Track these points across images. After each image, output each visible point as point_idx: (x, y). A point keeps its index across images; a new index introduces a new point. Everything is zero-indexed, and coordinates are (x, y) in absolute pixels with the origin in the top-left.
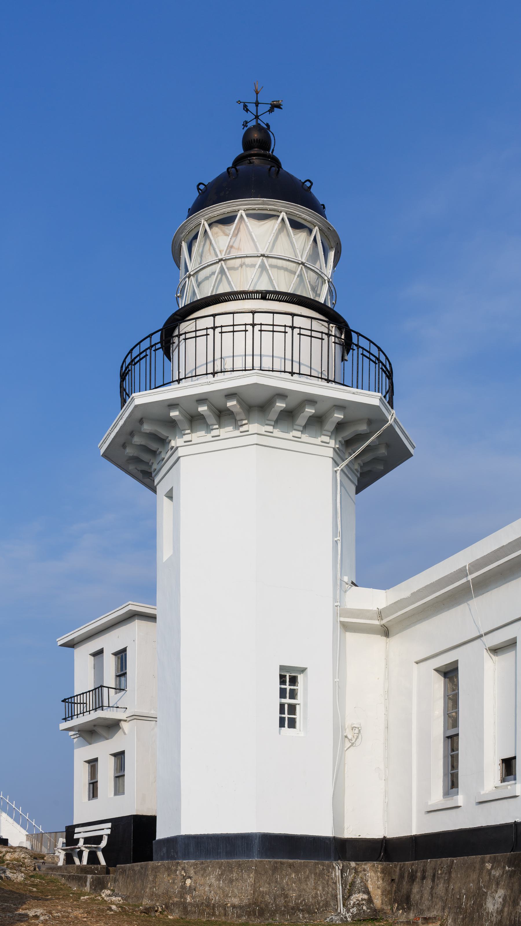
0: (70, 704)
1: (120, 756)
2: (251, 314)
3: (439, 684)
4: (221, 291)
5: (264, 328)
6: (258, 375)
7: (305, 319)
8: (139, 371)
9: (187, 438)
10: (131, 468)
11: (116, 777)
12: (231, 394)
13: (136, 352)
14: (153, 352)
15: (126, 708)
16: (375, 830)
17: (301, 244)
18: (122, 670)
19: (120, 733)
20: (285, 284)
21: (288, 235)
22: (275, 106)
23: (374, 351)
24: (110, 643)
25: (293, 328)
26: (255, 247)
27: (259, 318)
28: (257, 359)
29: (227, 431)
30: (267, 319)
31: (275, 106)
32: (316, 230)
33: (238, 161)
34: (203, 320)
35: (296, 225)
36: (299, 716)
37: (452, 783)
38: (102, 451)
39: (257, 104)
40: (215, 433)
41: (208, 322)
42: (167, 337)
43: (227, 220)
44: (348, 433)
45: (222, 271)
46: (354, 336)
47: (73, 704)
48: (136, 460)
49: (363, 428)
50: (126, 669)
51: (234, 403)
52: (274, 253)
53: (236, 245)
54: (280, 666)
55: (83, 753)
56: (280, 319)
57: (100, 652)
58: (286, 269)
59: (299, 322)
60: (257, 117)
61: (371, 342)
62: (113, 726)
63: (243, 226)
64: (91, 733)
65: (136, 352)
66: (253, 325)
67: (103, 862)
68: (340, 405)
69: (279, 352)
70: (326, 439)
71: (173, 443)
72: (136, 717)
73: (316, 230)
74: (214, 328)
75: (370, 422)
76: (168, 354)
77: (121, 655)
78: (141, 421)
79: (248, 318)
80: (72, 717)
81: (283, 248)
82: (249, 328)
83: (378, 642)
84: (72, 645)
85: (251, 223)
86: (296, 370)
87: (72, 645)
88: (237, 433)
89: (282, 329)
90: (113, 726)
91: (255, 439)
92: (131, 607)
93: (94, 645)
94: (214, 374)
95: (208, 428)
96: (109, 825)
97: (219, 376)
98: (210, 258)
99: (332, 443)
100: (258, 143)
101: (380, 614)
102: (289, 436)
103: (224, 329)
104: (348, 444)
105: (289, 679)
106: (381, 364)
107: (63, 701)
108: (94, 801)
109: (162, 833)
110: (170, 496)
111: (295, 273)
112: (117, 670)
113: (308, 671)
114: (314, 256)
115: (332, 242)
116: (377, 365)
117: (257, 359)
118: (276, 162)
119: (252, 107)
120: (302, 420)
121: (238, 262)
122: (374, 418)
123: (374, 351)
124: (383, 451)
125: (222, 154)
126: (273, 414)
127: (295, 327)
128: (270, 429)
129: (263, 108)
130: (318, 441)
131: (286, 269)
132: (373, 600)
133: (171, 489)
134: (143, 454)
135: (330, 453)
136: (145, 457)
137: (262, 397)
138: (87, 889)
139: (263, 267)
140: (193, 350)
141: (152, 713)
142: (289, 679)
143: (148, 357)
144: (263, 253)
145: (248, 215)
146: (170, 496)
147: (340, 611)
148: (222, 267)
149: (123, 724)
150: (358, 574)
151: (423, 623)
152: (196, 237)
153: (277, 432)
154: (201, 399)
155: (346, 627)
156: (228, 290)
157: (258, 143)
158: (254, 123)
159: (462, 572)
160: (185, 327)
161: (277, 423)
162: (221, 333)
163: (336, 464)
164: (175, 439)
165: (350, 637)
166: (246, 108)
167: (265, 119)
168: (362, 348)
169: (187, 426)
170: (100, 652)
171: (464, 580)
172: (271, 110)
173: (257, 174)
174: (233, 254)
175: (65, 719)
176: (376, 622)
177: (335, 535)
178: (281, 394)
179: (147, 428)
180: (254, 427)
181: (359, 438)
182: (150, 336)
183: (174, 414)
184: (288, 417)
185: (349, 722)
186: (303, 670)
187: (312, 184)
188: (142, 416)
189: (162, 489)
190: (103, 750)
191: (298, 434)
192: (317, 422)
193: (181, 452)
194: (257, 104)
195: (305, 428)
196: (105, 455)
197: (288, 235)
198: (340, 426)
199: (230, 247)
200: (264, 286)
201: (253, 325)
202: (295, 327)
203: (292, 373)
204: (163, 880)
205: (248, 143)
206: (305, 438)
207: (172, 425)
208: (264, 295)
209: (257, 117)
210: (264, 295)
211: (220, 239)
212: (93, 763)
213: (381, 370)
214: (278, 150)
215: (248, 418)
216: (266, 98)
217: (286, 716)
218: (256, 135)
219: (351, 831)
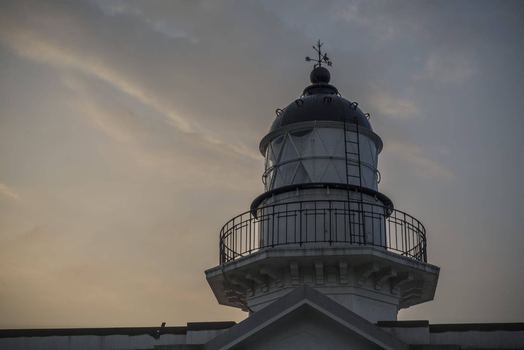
0: (361, 210)
2: (299, 204)
5: (308, 212)
14: (235, 231)
30: (283, 208)
31: (308, 59)
41: (270, 210)
47: (361, 210)
61: (413, 218)
65: (225, 230)
74: (301, 211)
79: (297, 207)
89: (323, 212)
100: (320, 78)
103: (281, 215)
106: (407, 224)
116: (403, 226)
123: (416, 224)
127: (332, 209)
143: (232, 234)
144: (331, 155)
145: (292, 135)
157: (320, 78)
162: (278, 217)
168: (408, 223)
187: (357, 104)
202: (332, 209)
213: (407, 229)
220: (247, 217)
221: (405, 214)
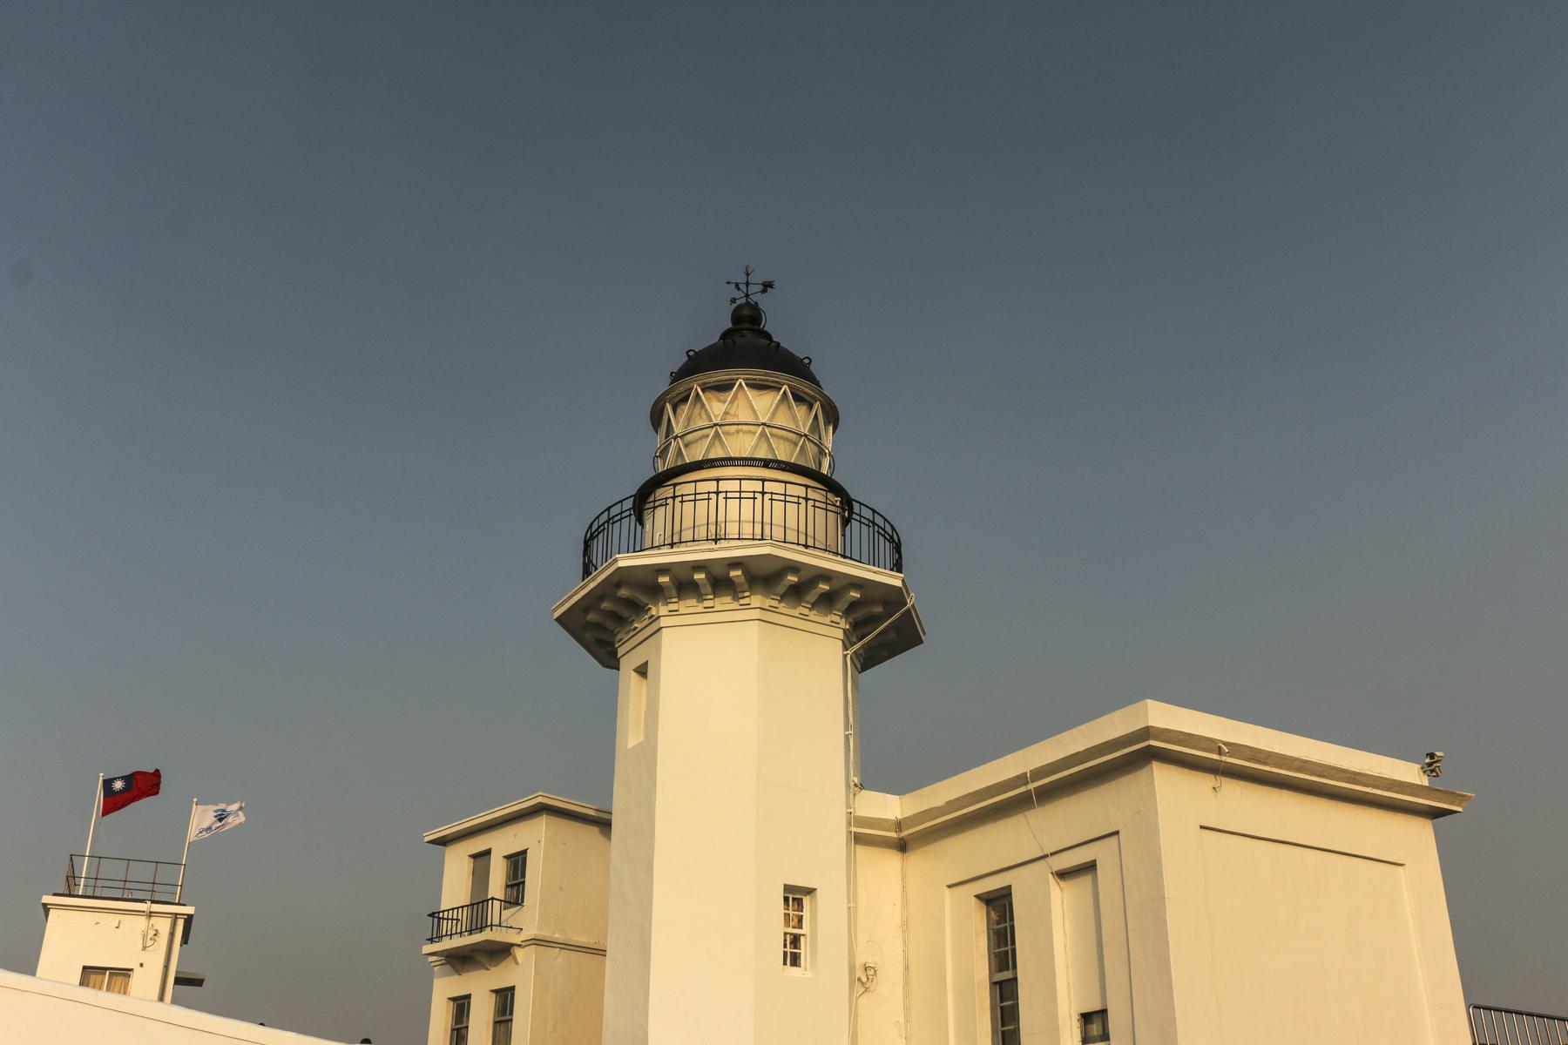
1: (505, 998)
3: (977, 922)
4: (712, 456)
6: (772, 545)
7: (796, 487)
8: (598, 546)
9: (672, 607)
10: (588, 635)
11: (496, 1023)
12: (735, 563)
15: (1117, 833)
17: (801, 418)
18: (515, 877)
19: (509, 961)
20: (783, 454)
21: (790, 407)
22: (767, 286)
24: (502, 844)
26: (748, 415)
27: (769, 487)
28: (712, 528)
29: (724, 602)
31: (767, 286)
32: (817, 405)
33: (725, 336)
34: (702, 484)
35: (799, 399)
36: (804, 950)
38: (556, 615)
39: (747, 284)
40: (707, 603)
42: (642, 500)
43: (724, 387)
44: (859, 614)
45: (717, 435)
46: (856, 507)
48: (597, 626)
49: (879, 609)
50: (523, 875)
51: (739, 573)
52: (774, 423)
53: (732, 412)
55: (445, 987)
57: (488, 853)
58: (787, 439)
59: (811, 494)
62: (500, 952)
63: (740, 395)
64: (461, 960)
66: (763, 493)
68: (859, 584)
69: (792, 523)
70: (837, 619)
71: (654, 612)
72: (537, 942)
73: (817, 405)
74: (717, 493)
75: (886, 604)
76: (640, 521)
77: (517, 862)
78: (618, 585)
81: (782, 420)
83: (892, 860)
84: (444, 842)
85: (749, 392)
86: (810, 543)
87: (444, 842)
88: (735, 605)
90: (500, 952)
91: (756, 614)
92: (540, 800)
93: (477, 844)
94: (716, 540)
95: (700, 597)
97: (723, 544)
98: (704, 423)
99: (844, 624)
100: (747, 319)
101: (899, 825)
102: (796, 612)
104: (856, 626)
105: (795, 896)
110: (642, 671)
111: (796, 444)
112: (508, 878)
113: (818, 892)
114: (815, 427)
115: (832, 415)
117: (767, 528)
118: (768, 336)
119: (743, 287)
120: (812, 596)
121: (734, 428)
122: (893, 599)
123: (867, 513)
124: (893, 636)
125: (711, 328)
126: (781, 589)
128: (775, 603)
129: (752, 289)
130: (827, 620)
131: (787, 439)
132: (888, 807)
133: (646, 664)
134: (608, 622)
135: (840, 634)
136: (610, 624)
139: (763, 434)
140: (658, 521)
142: (795, 896)
146: (642, 671)
147: (853, 820)
148: (717, 433)
149: (519, 954)
150: (862, 777)
151: (930, 847)
152: (685, 399)
153: (782, 607)
154: (698, 566)
155: (859, 839)
156: (722, 455)
157: (747, 319)
158: (743, 301)
159: (1021, 779)
160: (664, 492)
161: (783, 598)
163: (845, 648)
164: (656, 604)
165: (862, 851)
166: (737, 286)
167: (754, 298)
169: (674, 592)
170: (488, 853)
171: (1022, 789)
172: (764, 291)
173: (748, 345)
174: (730, 420)
175: (431, 940)
176: (894, 835)
177: (846, 728)
178: (794, 567)
179: (623, 592)
180: (756, 600)
181: (874, 620)
182: (608, 509)
183: (664, 579)
184: (795, 594)
185: (859, 962)
186: (810, 891)
188: (623, 577)
189: (628, 664)
190: (480, 986)
191: (806, 611)
192: (826, 602)
193: (663, 622)
194: (747, 284)
195: (814, 606)
196: (559, 620)
197: (790, 407)
198: (853, 606)
199: (726, 413)
200: (762, 453)
201: (763, 493)
203: (806, 546)
205: (737, 317)
206: (813, 615)
207: (657, 592)
208: (766, 464)
209: (747, 296)
210: (766, 464)
211: (716, 407)
212: (461, 1005)
214: (769, 326)
215: (750, 590)
216: (758, 278)
217: (788, 950)
218: (746, 312)
221: (874, 511)
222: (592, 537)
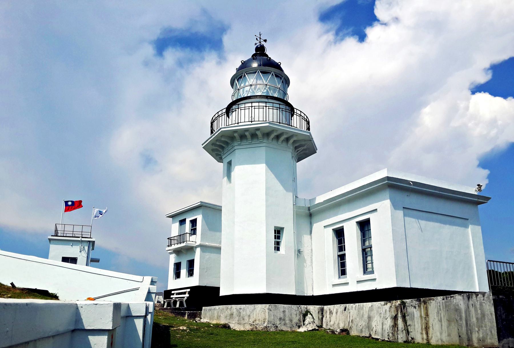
4: (249, 95)
13: (220, 113)
16: (317, 292)
22: (265, 41)
23: (305, 117)
25: (280, 108)
30: (257, 104)
37: (343, 272)
39: (260, 38)
54: (275, 227)
56: (261, 104)
60: (260, 42)
65: (220, 113)
66: (252, 107)
67: (185, 306)
80: (171, 245)
82: (250, 108)
96: (189, 290)
104: (296, 148)
107: (168, 239)
108: (178, 280)
109: (222, 293)
119: (259, 39)
123: (305, 117)
137: (267, 131)
138: (186, 317)
141: (282, 247)
167: (263, 43)
175: (168, 246)
198: (295, 142)
204: (211, 315)
209: (260, 42)
214: (268, 52)
216: (263, 38)
219: (309, 293)
220: (224, 111)
222: (213, 122)
